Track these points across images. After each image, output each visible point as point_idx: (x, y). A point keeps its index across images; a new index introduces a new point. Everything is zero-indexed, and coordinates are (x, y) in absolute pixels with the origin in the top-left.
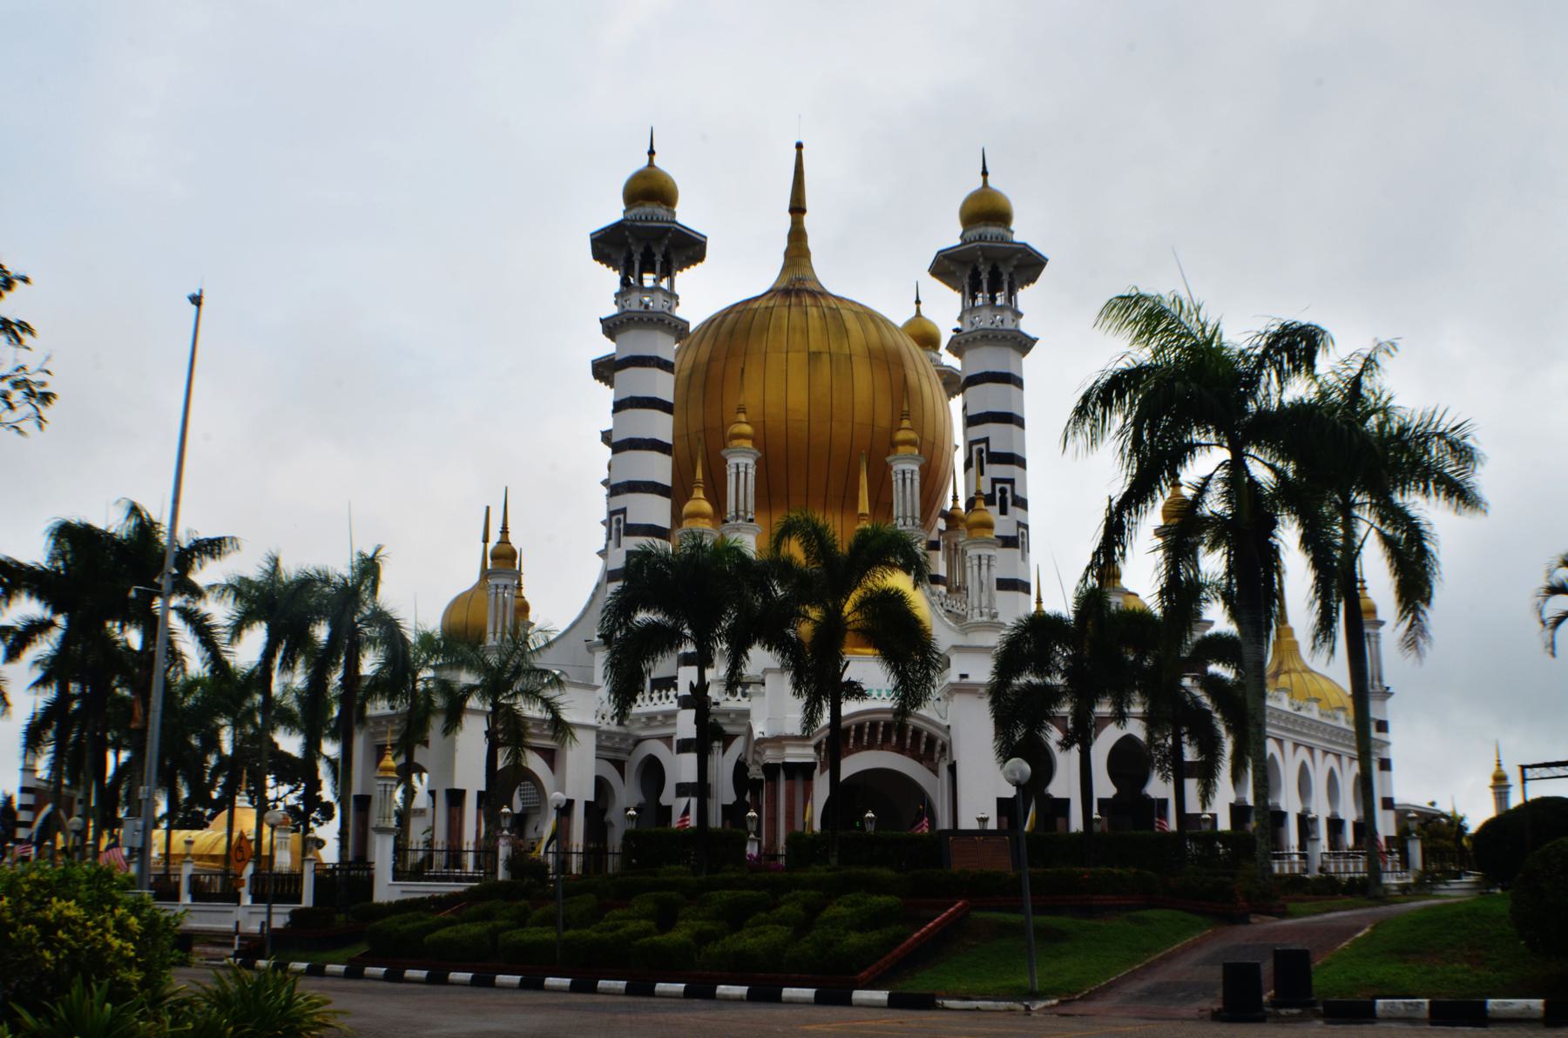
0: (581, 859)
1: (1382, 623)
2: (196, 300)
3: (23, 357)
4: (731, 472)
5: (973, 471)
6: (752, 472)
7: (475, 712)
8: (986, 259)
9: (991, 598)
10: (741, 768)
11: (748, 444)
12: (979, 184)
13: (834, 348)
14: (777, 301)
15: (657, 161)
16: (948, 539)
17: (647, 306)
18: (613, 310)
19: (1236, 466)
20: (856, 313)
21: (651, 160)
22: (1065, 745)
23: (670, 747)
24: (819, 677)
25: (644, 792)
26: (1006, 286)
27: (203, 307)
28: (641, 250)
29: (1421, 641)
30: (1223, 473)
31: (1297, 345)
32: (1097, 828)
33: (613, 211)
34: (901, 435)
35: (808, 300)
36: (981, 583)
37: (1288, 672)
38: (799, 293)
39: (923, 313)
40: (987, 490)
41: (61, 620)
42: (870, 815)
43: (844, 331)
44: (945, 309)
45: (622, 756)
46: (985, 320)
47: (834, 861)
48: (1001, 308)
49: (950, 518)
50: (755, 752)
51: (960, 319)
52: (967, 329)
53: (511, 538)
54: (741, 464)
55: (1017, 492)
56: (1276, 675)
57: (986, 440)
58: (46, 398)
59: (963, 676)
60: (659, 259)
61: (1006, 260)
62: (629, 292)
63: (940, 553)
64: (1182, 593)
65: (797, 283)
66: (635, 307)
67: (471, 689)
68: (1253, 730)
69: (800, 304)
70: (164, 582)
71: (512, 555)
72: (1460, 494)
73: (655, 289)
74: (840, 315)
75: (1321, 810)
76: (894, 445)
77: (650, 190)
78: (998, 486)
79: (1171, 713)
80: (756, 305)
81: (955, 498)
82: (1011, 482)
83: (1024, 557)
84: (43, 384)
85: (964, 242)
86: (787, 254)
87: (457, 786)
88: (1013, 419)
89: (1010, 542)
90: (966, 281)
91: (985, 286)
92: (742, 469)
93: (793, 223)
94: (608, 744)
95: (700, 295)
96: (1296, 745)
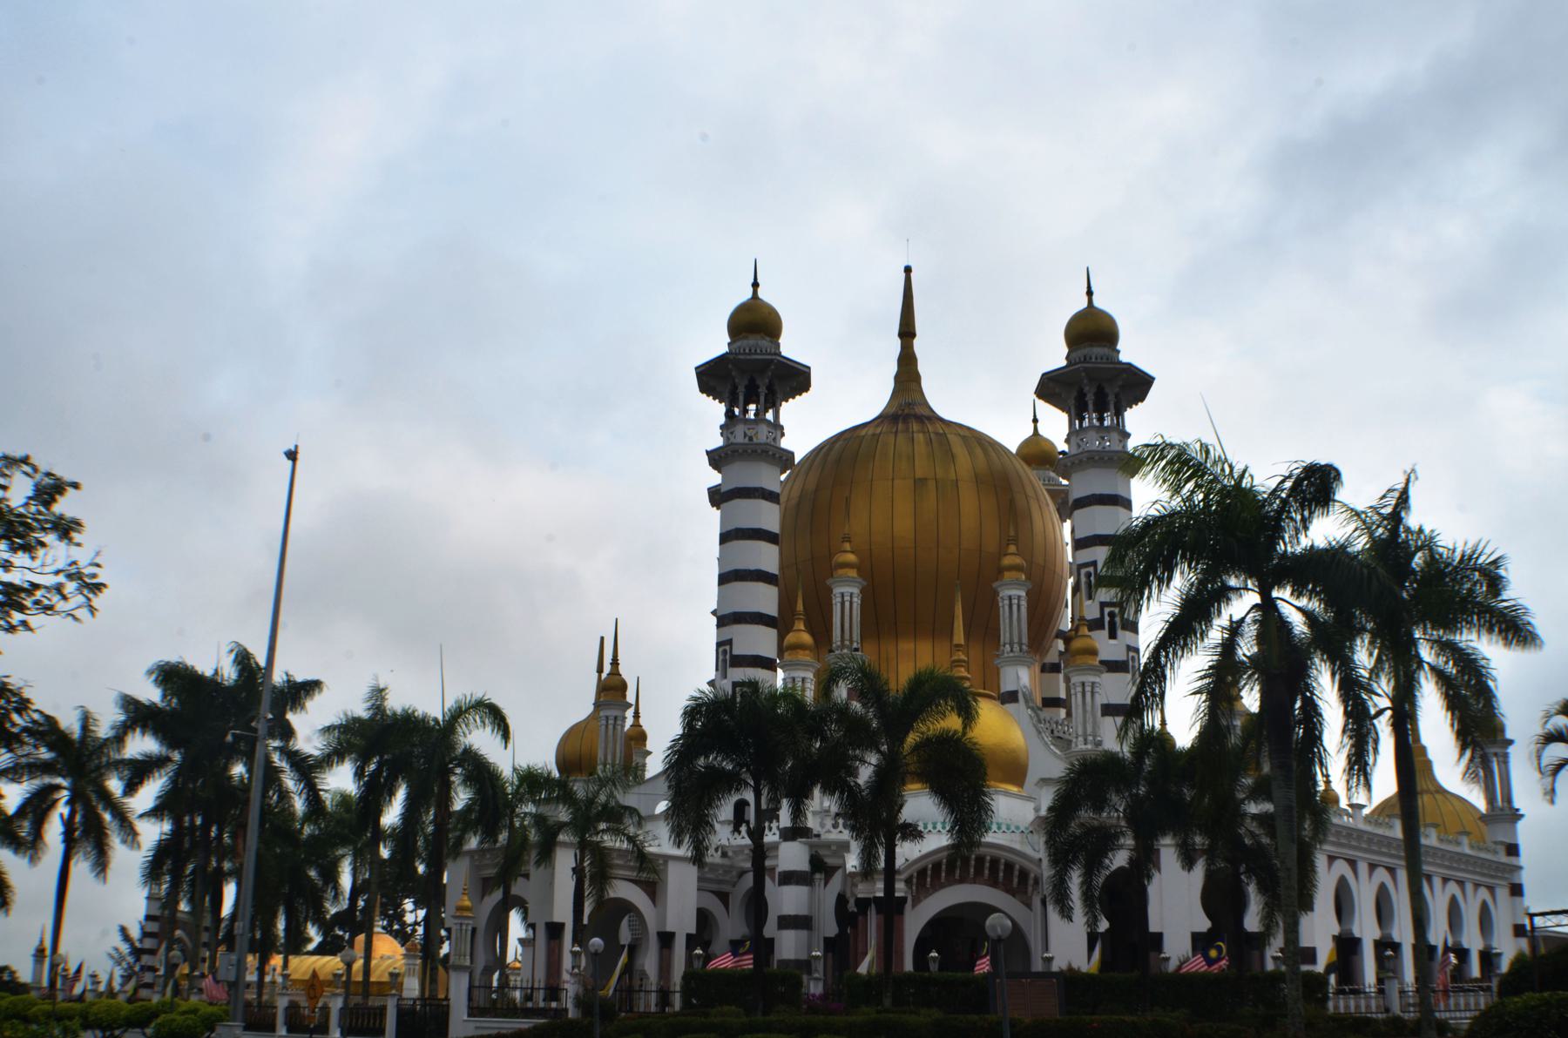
1: (1511, 742)
2: (292, 455)
3: (76, 553)
4: (837, 601)
7: (565, 844)
9: (1095, 725)
10: (841, 900)
11: (853, 573)
15: (761, 294)
18: (717, 441)
19: (1268, 607)
20: (964, 438)
27: (299, 463)
31: (1317, 485)
33: (718, 344)
34: (1007, 561)
35: (915, 426)
39: (1041, 431)
41: (176, 756)
42: (934, 954)
43: (951, 457)
44: (1056, 426)
45: (725, 888)
47: (887, 1002)
54: (847, 594)
58: (97, 588)
60: (763, 391)
69: (906, 430)
70: (260, 727)
72: (1515, 629)
75: (1473, 941)
76: (1000, 571)
77: (755, 322)
78: (1107, 610)
80: (863, 432)
84: (94, 576)
90: (1072, 402)
91: (1091, 407)
92: (847, 598)
95: (804, 426)
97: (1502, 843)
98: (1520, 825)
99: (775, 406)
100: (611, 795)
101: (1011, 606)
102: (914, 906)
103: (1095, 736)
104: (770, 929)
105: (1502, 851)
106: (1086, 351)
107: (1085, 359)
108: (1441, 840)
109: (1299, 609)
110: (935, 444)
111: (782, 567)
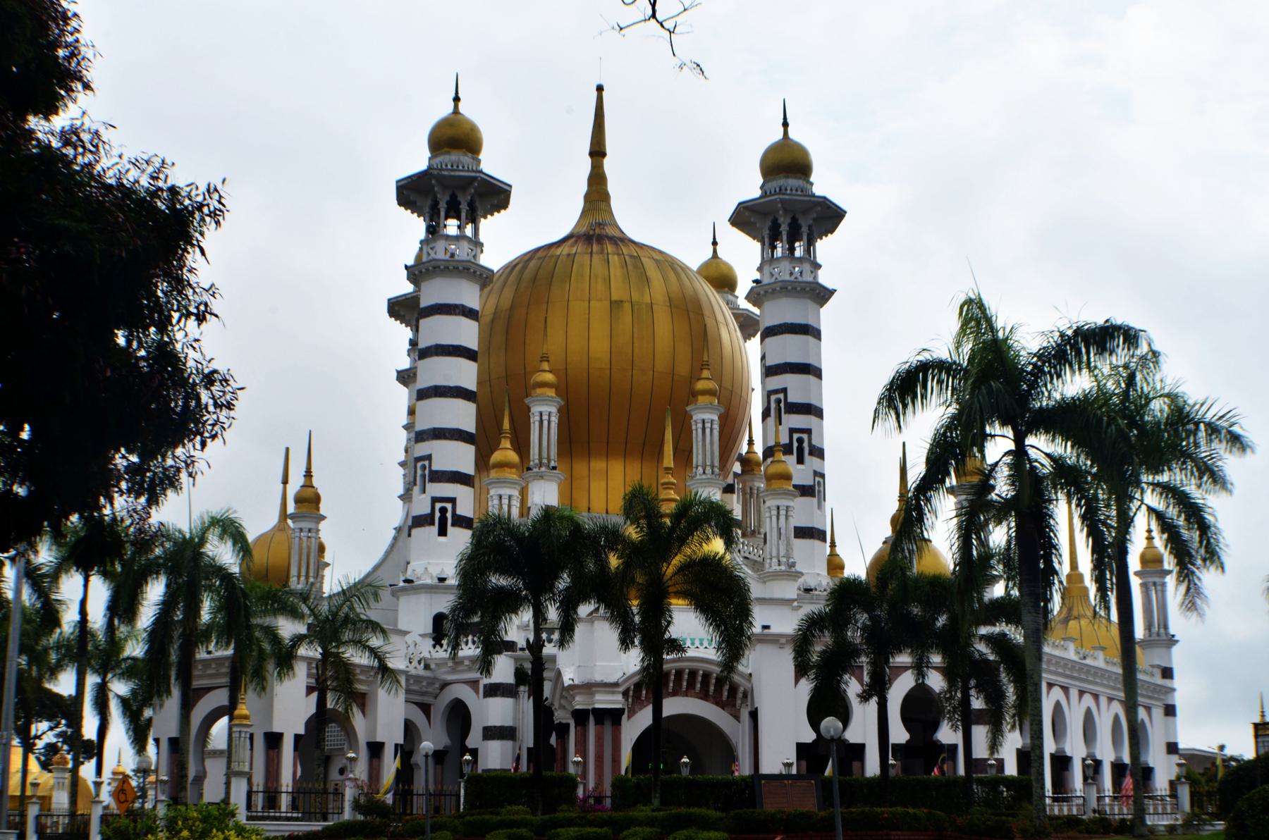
0: (290, 798)
1: (323, 518)
4: (535, 419)
5: (771, 420)
6: (554, 420)
8: (786, 211)
9: (789, 547)
11: (551, 393)
12: (780, 136)
13: (636, 296)
14: (580, 247)
16: (744, 483)
17: (452, 255)
19: (1020, 453)
20: (657, 261)
21: (456, 107)
22: (865, 697)
23: (477, 691)
24: (650, 634)
25: (450, 734)
26: (805, 238)
28: (447, 198)
29: (1198, 602)
30: (1008, 459)
32: (892, 773)
34: (701, 385)
35: (610, 248)
36: (779, 529)
37: (1078, 618)
38: (601, 239)
39: (720, 254)
40: (784, 439)
42: (685, 760)
43: (645, 280)
44: (744, 256)
45: (428, 700)
46: (783, 272)
47: (656, 802)
48: (800, 259)
49: (748, 463)
50: (562, 697)
51: (760, 269)
52: (766, 280)
53: (315, 482)
54: (545, 412)
55: (814, 442)
56: (1066, 621)
57: (784, 391)
59: (766, 627)
60: (464, 207)
61: (805, 212)
62: (434, 240)
63: (735, 496)
64: (974, 566)
65: (596, 228)
66: (441, 255)
67: (298, 640)
68: (1030, 688)
69: (602, 252)
71: (316, 499)
73: (461, 237)
74: (641, 260)
76: (694, 395)
77: (455, 137)
78: (796, 436)
79: (962, 669)
81: (751, 442)
82: (808, 431)
83: (820, 506)
85: (765, 194)
86: (587, 197)
87: (276, 729)
88: (811, 370)
89: (806, 491)
90: (766, 232)
91: (785, 237)
92: (545, 417)
93: (593, 167)
94: (415, 688)
95: (502, 241)
96: (1081, 693)
97: (1158, 666)
98: (1175, 649)
99: (474, 220)
100: (352, 608)
101: (704, 429)
102: (629, 717)
103: (788, 558)
104: (474, 739)
105: (1158, 673)
106: (781, 182)
107: (781, 190)
108: (1107, 663)
109: (1048, 455)
110: (630, 267)
111: (479, 383)
